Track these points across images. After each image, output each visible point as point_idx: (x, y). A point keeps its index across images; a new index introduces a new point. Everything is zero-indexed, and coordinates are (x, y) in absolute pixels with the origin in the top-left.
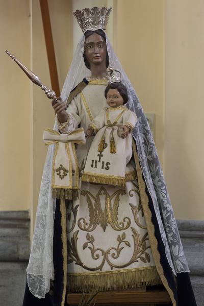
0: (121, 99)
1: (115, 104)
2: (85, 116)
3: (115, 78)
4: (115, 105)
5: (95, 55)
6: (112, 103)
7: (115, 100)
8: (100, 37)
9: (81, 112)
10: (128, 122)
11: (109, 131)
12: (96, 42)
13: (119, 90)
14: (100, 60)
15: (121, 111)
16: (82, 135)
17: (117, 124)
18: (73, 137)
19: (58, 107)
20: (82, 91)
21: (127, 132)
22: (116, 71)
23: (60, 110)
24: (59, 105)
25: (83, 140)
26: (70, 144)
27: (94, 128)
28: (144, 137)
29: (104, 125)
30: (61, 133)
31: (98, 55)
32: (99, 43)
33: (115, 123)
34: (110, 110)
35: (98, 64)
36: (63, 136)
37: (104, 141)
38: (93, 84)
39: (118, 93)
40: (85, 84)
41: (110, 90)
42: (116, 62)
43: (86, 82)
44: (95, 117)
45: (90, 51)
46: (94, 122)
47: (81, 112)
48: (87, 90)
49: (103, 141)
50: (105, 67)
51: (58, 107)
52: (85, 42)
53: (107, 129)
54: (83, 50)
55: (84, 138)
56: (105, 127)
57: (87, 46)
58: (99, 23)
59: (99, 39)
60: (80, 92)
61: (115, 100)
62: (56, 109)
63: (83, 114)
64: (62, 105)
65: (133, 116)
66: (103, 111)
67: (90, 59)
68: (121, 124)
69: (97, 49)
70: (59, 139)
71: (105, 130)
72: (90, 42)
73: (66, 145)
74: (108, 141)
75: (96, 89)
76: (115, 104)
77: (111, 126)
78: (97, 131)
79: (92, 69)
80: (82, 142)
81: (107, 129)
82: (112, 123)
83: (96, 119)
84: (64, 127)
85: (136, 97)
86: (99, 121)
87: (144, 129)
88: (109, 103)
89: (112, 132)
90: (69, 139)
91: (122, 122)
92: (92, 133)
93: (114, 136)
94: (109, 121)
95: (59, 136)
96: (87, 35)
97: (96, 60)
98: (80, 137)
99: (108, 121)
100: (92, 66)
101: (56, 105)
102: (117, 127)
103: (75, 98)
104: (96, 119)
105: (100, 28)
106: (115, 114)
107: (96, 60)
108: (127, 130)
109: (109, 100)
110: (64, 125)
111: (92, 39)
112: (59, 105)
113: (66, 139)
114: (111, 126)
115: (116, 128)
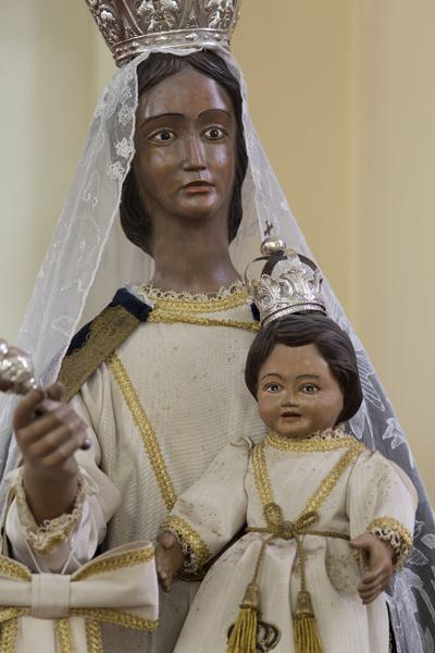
0: (332, 397)
1: (304, 423)
2: (135, 475)
3: (291, 294)
4: (293, 426)
5: (187, 178)
6: (286, 415)
7: (304, 401)
8: (212, 84)
9: (117, 456)
10: (382, 514)
11: (281, 559)
12: (194, 111)
13: (328, 352)
14: (212, 200)
15: (336, 456)
16: (143, 581)
17: (322, 525)
18: (97, 589)
19: (51, 438)
20: (121, 355)
21: (385, 571)
22: (304, 259)
23: (63, 450)
24: (57, 424)
25: (148, 606)
26: (78, 626)
27: (194, 542)
28: (419, 587)
29: (242, 531)
30: (34, 571)
31: (206, 176)
32: (209, 116)
33: (309, 520)
34: (269, 451)
35: (197, 220)
36: (49, 587)
37: (258, 611)
38: (169, 321)
39: (321, 366)
40: (131, 318)
41: (281, 351)
42: (282, 213)
43: (130, 310)
44: (186, 486)
45: (161, 158)
46: (189, 510)
47: (117, 456)
48: (143, 348)
49: (253, 609)
50: (224, 237)
51: (51, 438)
52: (139, 113)
53: (269, 551)
54: (126, 149)
55: (153, 595)
56: (251, 543)
57: (151, 131)
58: (203, 20)
59: (209, 98)
60: (110, 357)
61: (304, 401)
62: (37, 447)
63: (126, 469)
64: (72, 426)
65: (404, 489)
66: (234, 458)
67: (163, 193)
68: (339, 525)
69: (199, 150)
70: (22, 599)
71: (262, 554)
72: (158, 111)
73: (56, 629)
74: (279, 613)
75: (186, 355)
76: (304, 423)
77: (284, 531)
78: (209, 560)
79: (159, 241)
80: (145, 615)
81: (269, 551)
82: (292, 515)
83: (190, 496)
84: (57, 541)
85: (379, 390)
86: (211, 506)
87: (169, 549)
88: (271, 421)
89: (299, 568)
90: (75, 601)
91: (344, 515)
92: (187, 570)
93: (311, 588)
94: (276, 507)
95: (22, 586)
96: (153, 72)
97: (193, 202)
98: (134, 592)
99: (272, 508)
100: (164, 230)
101: (38, 425)
102: (320, 541)
103: (85, 388)
104: (190, 496)
105: (211, 44)
106: (303, 473)
107: (193, 202)
108: (382, 557)
109: (273, 400)
110: (57, 526)
111: (163, 100)
112: (57, 424)
113: (63, 601)
114: (284, 531)
115: (312, 541)
